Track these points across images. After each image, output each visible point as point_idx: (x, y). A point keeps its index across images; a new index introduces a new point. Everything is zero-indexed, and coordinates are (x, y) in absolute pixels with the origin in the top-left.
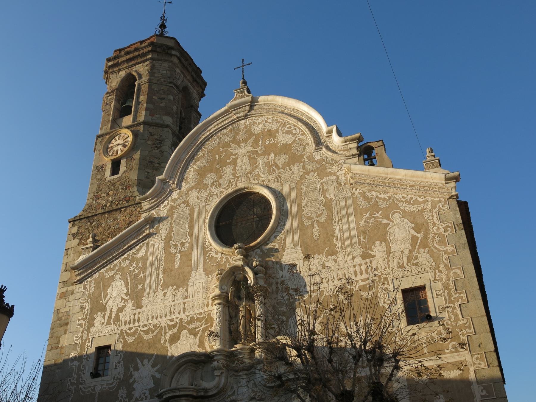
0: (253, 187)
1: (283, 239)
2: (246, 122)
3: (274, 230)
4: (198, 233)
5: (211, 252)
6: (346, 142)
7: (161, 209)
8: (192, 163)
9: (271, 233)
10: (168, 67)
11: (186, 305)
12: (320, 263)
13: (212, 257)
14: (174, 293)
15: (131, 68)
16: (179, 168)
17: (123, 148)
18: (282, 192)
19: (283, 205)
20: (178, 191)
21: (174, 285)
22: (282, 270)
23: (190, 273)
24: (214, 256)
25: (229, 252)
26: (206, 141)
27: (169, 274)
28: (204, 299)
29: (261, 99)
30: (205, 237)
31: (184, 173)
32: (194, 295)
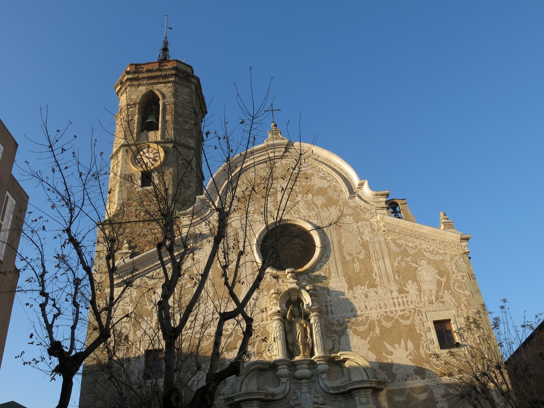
0: (296, 221)
1: (328, 268)
15: (152, 86)
17: (153, 162)
22: (330, 295)
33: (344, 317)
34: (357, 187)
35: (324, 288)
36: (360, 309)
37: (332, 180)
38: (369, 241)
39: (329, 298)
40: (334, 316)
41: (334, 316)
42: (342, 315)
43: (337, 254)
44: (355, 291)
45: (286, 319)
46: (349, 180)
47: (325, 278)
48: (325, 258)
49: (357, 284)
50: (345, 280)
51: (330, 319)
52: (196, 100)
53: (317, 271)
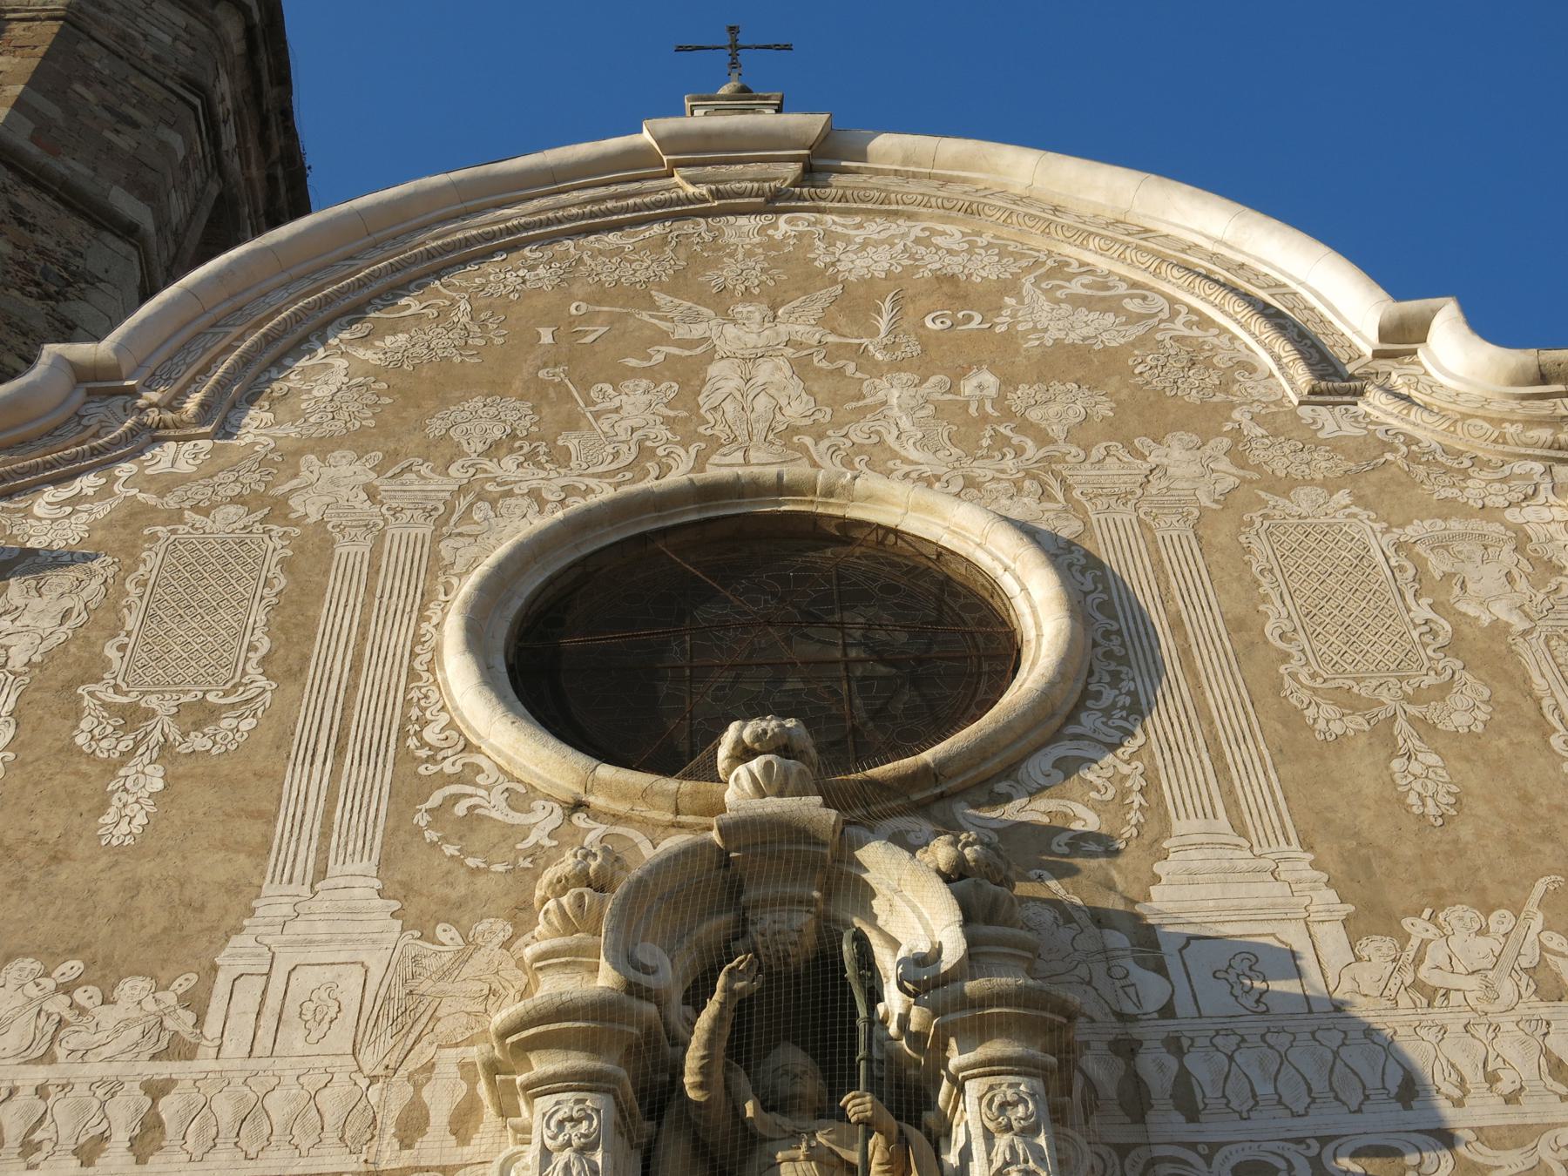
0: (848, 491)
1: (1137, 782)
2: (774, 226)
3: (1056, 723)
4: (355, 669)
5: (468, 789)
6: (1543, 378)
7: (37, 510)
8: (345, 335)
9: (1034, 737)
10: (185, 30)
11: (169, 1107)
12: (1506, 962)
13: (474, 818)
14: (58, 1006)
16: (229, 349)
18: (1088, 545)
19: (1106, 608)
20: (206, 444)
21: (73, 952)
22: (1161, 969)
23: (242, 894)
24: (494, 814)
25: (645, 794)
26: (464, 262)
27: (34, 877)
28: (373, 1079)
29: (887, 146)
30: (415, 694)
31: (266, 370)
32: (265, 1039)
33: (1324, 1141)
34: (1368, 352)
35: (1100, 918)
36: (1492, 1079)
37: (1165, 315)
38: (1519, 624)
39: (1152, 990)
40: (1212, 1129)
41: (1212, 1129)
42: (1302, 1127)
43: (1222, 691)
44: (1424, 943)
45: (671, 1114)
46: (1298, 317)
47: (1104, 846)
48: (1107, 712)
49: (1439, 900)
50: (1314, 865)
51: (1159, 1151)
52: (241, 148)
53: (1032, 795)
